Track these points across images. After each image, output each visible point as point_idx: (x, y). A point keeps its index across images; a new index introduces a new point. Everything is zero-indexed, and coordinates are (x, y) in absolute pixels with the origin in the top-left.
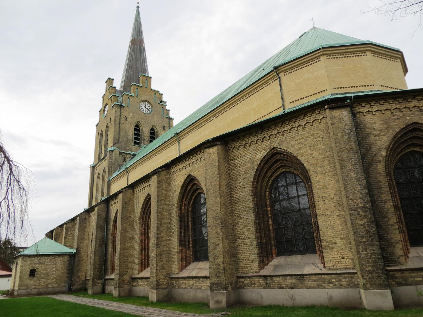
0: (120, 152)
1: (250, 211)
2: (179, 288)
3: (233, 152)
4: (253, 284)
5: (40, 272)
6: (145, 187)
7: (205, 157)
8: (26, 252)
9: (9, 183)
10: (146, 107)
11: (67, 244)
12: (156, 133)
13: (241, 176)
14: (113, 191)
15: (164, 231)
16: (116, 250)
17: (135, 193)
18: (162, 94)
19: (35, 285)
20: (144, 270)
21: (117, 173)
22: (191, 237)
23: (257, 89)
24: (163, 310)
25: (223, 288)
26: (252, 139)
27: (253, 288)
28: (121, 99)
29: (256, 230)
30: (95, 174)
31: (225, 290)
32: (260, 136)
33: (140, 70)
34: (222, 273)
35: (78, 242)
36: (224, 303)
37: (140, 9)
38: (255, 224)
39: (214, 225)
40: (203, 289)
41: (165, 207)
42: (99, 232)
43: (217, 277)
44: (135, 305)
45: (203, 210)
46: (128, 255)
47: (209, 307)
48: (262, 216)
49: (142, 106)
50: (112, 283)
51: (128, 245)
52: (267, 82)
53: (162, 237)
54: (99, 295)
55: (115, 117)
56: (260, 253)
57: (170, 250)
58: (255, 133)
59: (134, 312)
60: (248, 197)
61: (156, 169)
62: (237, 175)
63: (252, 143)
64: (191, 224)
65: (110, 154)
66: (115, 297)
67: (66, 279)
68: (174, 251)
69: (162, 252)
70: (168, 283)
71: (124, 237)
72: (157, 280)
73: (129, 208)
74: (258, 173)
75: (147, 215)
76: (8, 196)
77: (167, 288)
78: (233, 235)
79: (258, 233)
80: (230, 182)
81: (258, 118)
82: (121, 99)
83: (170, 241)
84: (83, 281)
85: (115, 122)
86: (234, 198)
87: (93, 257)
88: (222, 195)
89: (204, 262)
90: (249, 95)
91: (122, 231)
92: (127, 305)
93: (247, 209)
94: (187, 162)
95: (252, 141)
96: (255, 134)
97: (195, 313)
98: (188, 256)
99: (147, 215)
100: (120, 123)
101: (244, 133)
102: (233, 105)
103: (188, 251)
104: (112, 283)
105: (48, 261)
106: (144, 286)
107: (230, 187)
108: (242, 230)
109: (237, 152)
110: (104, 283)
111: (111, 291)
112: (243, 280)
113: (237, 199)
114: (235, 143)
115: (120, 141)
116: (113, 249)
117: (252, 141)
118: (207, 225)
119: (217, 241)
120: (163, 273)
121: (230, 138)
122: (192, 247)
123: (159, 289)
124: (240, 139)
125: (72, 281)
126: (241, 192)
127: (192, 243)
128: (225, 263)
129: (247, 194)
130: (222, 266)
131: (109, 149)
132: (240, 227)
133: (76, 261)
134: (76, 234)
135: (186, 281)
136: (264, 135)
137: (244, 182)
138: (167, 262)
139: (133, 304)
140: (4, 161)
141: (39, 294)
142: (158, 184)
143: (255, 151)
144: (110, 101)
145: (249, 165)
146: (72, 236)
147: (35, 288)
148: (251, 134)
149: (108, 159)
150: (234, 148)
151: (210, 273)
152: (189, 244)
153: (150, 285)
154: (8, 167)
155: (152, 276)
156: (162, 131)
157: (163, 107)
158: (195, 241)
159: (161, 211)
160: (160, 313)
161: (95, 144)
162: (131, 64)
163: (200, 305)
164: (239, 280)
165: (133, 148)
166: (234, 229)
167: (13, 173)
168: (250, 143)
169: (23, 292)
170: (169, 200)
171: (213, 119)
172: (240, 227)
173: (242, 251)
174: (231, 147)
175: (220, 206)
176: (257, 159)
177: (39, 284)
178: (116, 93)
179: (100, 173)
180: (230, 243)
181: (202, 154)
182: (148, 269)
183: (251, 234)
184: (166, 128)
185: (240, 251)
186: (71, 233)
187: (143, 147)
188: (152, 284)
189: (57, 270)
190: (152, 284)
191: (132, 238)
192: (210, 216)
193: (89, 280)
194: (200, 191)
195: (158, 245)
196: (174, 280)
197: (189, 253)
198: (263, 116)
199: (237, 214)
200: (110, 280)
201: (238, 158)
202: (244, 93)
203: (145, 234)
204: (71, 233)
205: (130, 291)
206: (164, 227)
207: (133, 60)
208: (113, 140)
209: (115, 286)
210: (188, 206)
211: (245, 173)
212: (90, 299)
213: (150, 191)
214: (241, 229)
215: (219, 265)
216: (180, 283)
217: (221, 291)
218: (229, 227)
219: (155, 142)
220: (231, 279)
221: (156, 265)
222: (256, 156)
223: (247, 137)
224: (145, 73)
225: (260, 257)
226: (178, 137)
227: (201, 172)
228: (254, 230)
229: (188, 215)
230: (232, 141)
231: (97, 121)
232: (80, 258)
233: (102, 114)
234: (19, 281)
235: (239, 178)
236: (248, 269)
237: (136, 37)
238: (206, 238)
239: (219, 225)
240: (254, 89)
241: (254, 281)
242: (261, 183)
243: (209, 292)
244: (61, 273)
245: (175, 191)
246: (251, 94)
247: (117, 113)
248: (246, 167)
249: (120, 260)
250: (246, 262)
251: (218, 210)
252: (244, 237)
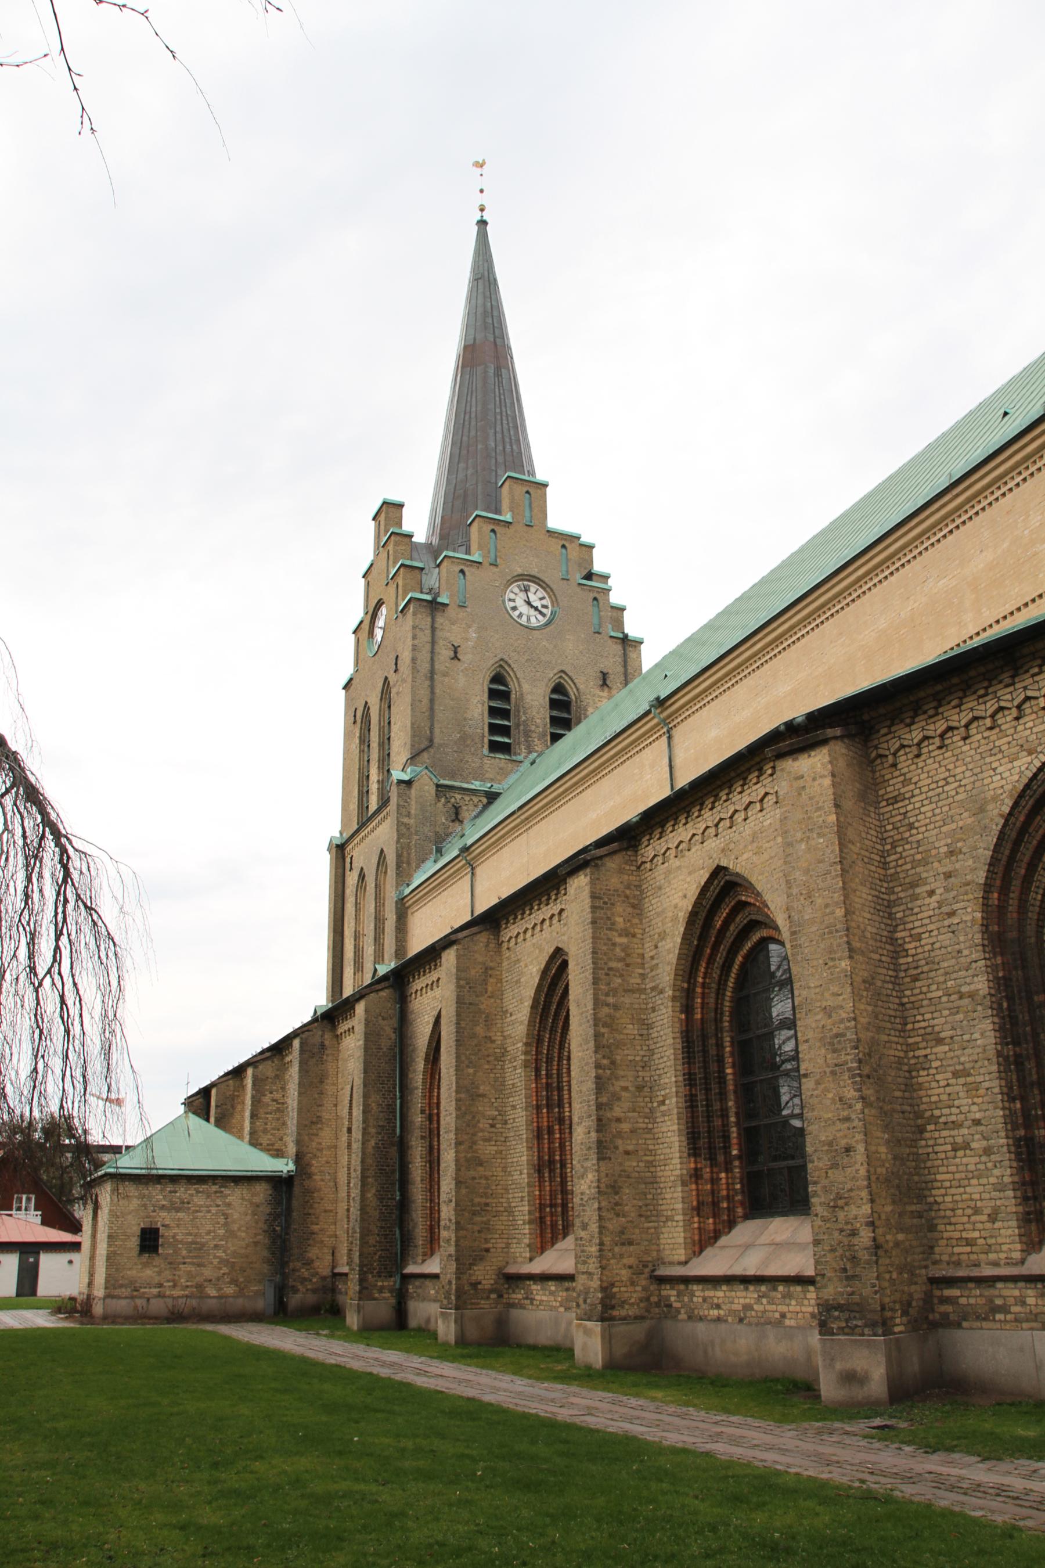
0: (438, 786)
1: (979, 1008)
2: (690, 1318)
3: (894, 765)
4: (1000, 1312)
5: (174, 1237)
6: (544, 920)
7: (781, 793)
8: (126, 1163)
9: (60, 917)
10: (529, 603)
11: (261, 1140)
12: (573, 704)
13: (936, 865)
14: (419, 941)
15: (623, 1094)
16: (443, 1165)
17: (505, 945)
18: (590, 547)
19: (160, 1285)
20: (553, 1244)
21: (430, 868)
22: (733, 1119)
23: (980, 497)
24: (634, 1402)
25: (873, 1325)
26: (972, 709)
27: (998, 1325)
28: (431, 580)
29: (1005, 1090)
30: (348, 873)
31: (880, 1331)
32: (1009, 697)
33: (500, 459)
34: (868, 1262)
35: (299, 1134)
36: (877, 1382)
37: (489, 228)
38: (999, 1064)
39: (828, 1070)
40: (791, 1327)
41: (627, 1000)
42: (375, 1098)
43: (848, 1278)
44: (521, 1376)
45: (780, 1008)
46: (488, 1187)
47: (819, 1397)
48: (1028, 1029)
49: (514, 601)
50: (432, 1292)
51: (487, 1150)
52: (1021, 468)
53: (618, 1120)
54: (384, 1334)
55: (415, 648)
56: (1024, 1184)
57: (652, 1169)
58: (986, 684)
59: (522, 1402)
60: (966, 952)
61: (584, 850)
62: (915, 863)
63: (975, 724)
64: (733, 1066)
65: (399, 796)
66: (446, 1344)
67: (266, 1268)
68: (665, 1173)
69: (620, 1176)
70: (648, 1299)
71: (468, 1117)
72: (605, 1284)
73: (485, 1004)
74: (1007, 852)
75: (553, 1030)
76: (60, 964)
77: (642, 1318)
78: (907, 1108)
79: (1012, 1100)
80: (891, 891)
81: (992, 621)
82: (431, 580)
83: (651, 1136)
84: (324, 1278)
85: (415, 669)
86: (910, 959)
87: (358, 1191)
88: (858, 945)
89: (792, 1218)
90: (951, 527)
91: (463, 1096)
92: (493, 1373)
93: (966, 1001)
94: (707, 814)
95: (976, 719)
96: (986, 688)
97: (761, 1418)
98: (724, 1193)
99: (553, 1030)
100: (432, 672)
101: (939, 687)
102: (887, 573)
103: (723, 1175)
104: (432, 1292)
105: (199, 1200)
106: (552, 1308)
107: (890, 914)
108: (948, 1090)
109: (913, 767)
110: (400, 1289)
111: (428, 1321)
112: (954, 1292)
113: (923, 962)
114: (901, 731)
115: (437, 740)
116: (431, 1162)
117: (976, 719)
118: (798, 1069)
119: (841, 1134)
120: (626, 1261)
121: (882, 711)
122: (739, 1157)
123: (612, 1319)
124: (925, 712)
125: (284, 1276)
126: (935, 933)
127: (740, 1144)
128: (877, 1223)
129: (962, 939)
130: (865, 1236)
131: (397, 774)
132: (938, 1077)
133: (295, 1203)
134: (290, 1101)
135: (720, 1294)
136: (1025, 688)
137: (947, 890)
138: (641, 1216)
139: (514, 1374)
140: (43, 836)
141: (176, 1317)
142: (594, 908)
143: (988, 760)
144: (392, 588)
145: (967, 820)
146: (278, 1110)
147: (160, 1295)
148: (969, 687)
149: (394, 815)
150: (898, 750)
151: (817, 1263)
152: (727, 1148)
153: (578, 1305)
154: (57, 858)
155: (582, 1268)
156: (598, 692)
157: (595, 599)
158: (750, 1136)
159: (609, 1016)
160: (626, 1410)
161: (344, 759)
162: (465, 439)
163: (780, 1387)
164: (937, 1293)
165: (486, 767)
166: (910, 1087)
167: (72, 880)
168: (967, 726)
169: (122, 1306)
170: (641, 971)
171: (804, 632)
172: (938, 1077)
173: (949, 1176)
174: (885, 746)
175: (849, 990)
176: (1000, 791)
177: (173, 1281)
178: (415, 555)
179: (365, 870)
180: (895, 1143)
181: (766, 780)
182: (569, 1242)
183: (985, 1107)
184: (615, 679)
185: (938, 1177)
186: (274, 1100)
187: (527, 763)
188: (585, 1302)
189: (231, 1234)
190: (585, 1302)
191: (500, 1121)
192: (810, 1035)
193: (346, 1275)
194: (765, 933)
195: (603, 1150)
196: (672, 1289)
197: (727, 1184)
198: (1013, 608)
199: (923, 1024)
200: (422, 1280)
201: (917, 792)
202: (927, 518)
203: (548, 1106)
204: (274, 1100)
205: (502, 1323)
206: (626, 1080)
207: (473, 423)
208: (409, 741)
209: (445, 1302)
210: (718, 994)
211: (951, 853)
212: (355, 1345)
213: (565, 938)
214: (942, 1083)
215: (854, 1233)
216: (695, 1299)
217: (863, 1335)
218: (890, 1079)
219: (570, 738)
220: (906, 1289)
221: (600, 1227)
222: (995, 779)
223: (953, 703)
224: (520, 468)
225: (1025, 1199)
226: (665, 714)
227: (766, 856)
228: (997, 1090)
229: (719, 1029)
230: (888, 723)
231: (346, 669)
232: (309, 1192)
233: (366, 643)
234: (108, 1267)
235: (924, 875)
236: (974, 1249)
237: (480, 336)
238: (797, 1123)
239: (849, 1069)
240: (969, 500)
241: (1004, 1297)
242: (1021, 893)
243: (815, 1338)
244: (248, 1246)
245: (663, 936)
246: (958, 521)
247: (420, 634)
248: (953, 826)
249: (457, 1205)
250: (965, 1219)
251: (842, 1007)
252: (953, 1118)
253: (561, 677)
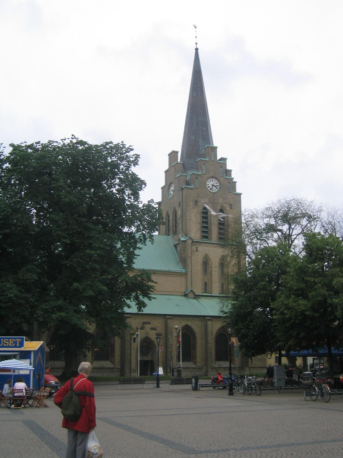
37: (198, 50)
253: (222, 207)
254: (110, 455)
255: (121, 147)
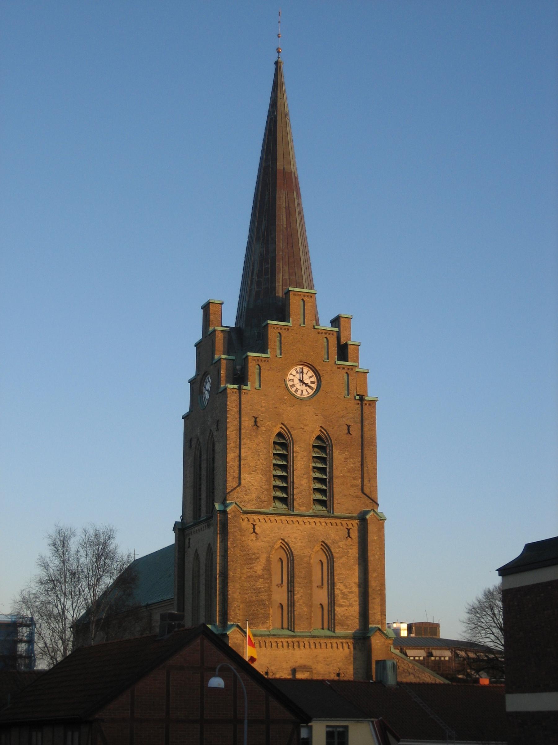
10: (302, 381)
254: (281, 99)
255: (91, 618)
